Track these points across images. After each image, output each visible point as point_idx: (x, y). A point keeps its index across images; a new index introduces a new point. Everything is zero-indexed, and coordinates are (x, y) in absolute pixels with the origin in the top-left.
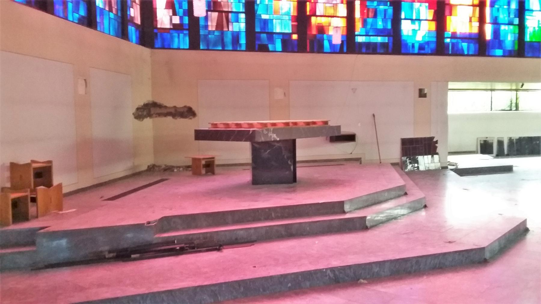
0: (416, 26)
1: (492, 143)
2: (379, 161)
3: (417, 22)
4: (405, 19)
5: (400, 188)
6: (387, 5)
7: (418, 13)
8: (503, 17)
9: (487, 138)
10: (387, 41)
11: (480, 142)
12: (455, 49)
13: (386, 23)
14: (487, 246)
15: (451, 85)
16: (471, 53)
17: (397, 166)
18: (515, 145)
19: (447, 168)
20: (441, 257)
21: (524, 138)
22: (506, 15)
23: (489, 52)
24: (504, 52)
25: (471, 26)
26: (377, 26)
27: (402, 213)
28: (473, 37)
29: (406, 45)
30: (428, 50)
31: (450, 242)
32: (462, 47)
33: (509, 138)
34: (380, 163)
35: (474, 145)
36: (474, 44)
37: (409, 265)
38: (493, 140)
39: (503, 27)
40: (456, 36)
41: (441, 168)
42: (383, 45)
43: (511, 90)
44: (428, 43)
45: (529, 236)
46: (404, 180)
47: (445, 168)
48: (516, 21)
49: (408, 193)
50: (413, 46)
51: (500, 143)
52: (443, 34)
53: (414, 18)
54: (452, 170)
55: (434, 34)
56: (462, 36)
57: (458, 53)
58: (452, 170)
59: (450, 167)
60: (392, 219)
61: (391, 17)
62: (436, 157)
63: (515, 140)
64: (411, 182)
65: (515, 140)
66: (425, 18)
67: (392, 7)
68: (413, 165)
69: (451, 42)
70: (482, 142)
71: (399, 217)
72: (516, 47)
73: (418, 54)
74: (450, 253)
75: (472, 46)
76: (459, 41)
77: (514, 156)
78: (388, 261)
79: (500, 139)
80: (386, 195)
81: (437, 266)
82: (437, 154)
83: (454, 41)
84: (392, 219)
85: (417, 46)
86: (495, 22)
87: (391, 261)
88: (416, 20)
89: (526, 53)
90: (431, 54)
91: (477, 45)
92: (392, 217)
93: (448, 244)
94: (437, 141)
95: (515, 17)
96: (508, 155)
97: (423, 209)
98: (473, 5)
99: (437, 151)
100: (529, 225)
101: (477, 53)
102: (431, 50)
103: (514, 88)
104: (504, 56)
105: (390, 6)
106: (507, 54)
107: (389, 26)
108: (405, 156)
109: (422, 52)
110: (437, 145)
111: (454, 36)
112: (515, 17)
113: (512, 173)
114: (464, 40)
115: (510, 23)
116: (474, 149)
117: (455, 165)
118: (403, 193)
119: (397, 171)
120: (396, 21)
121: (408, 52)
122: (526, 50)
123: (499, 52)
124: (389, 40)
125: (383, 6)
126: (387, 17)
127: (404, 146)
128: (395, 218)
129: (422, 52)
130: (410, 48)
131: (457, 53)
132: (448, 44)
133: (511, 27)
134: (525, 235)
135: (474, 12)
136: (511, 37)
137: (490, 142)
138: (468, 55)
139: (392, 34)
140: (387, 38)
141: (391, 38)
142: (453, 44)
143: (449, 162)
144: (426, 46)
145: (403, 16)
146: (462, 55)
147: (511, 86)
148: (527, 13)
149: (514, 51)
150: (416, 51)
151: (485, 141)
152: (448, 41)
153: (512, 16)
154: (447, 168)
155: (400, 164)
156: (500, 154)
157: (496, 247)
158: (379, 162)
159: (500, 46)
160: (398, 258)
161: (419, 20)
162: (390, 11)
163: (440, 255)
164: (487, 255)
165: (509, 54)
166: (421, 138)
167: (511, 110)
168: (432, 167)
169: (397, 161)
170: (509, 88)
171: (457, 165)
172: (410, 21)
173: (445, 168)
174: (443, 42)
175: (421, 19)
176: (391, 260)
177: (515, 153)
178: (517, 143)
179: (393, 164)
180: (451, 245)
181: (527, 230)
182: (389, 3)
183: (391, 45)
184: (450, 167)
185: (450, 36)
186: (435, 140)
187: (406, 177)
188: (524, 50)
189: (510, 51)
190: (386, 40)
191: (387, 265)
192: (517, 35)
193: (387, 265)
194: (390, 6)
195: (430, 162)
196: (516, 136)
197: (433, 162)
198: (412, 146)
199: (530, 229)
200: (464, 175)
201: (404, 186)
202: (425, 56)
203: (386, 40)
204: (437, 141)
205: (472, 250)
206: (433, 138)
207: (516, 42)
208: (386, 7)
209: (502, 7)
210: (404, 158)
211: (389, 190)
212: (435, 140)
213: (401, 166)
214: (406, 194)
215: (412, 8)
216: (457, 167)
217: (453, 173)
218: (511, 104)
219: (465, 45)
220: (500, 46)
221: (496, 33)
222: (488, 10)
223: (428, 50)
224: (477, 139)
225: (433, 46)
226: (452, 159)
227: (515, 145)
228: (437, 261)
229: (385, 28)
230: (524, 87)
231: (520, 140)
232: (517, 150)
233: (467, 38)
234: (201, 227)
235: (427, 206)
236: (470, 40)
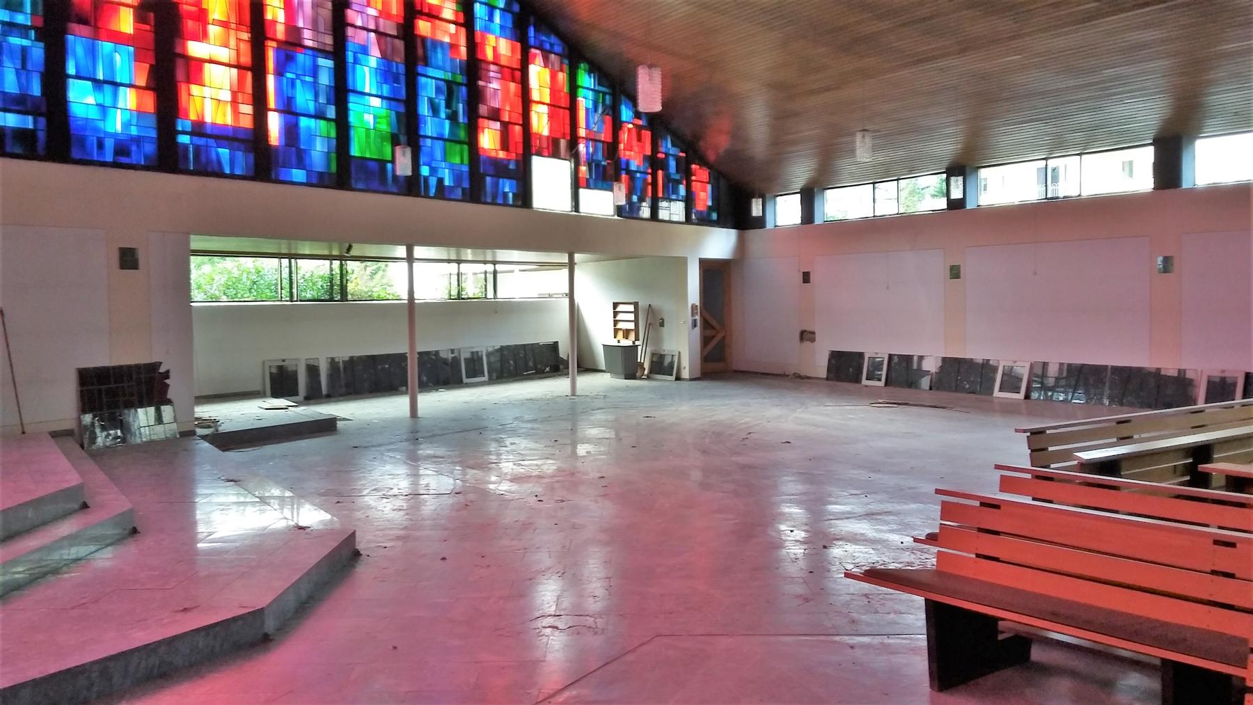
0: (106, 97)
1: (296, 372)
2: (20, 428)
3: (108, 88)
4: (78, 77)
5: (67, 494)
6: (27, 37)
7: (111, 65)
8: (304, 99)
9: (284, 361)
10: (31, 126)
11: (270, 369)
12: (203, 159)
13: (29, 81)
14: (270, 605)
15: (196, 242)
16: (238, 172)
17: (70, 438)
18: (342, 375)
19: (192, 433)
20: (163, 649)
21: (359, 358)
22: (310, 96)
23: (277, 175)
24: (310, 173)
25: (236, 112)
26: (3, 87)
27: (74, 557)
28: (242, 136)
29: (82, 141)
30: (136, 157)
31: (185, 610)
32: (218, 155)
33: (329, 360)
34: (24, 433)
35: (257, 376)
36: (246, 151)
37: (82, 681)
38: (297, 365)
39: (304, 122)
40: (204, 131)
41: (178, 436)
42: (21, 135)
43: (449, 261)
44: (138, 140)
45: (363, 571)
46: (82, 474)
47: (188, 434)
48: (331, 112)
49: (89, 505)
50: (101, 145)
51: (313, 370)
52: (174, 125)
53: (100, 76)
54: (204, 437)
55: (152, 121)
56: (215, 132)
57: (209, 170)
58: (204, 437)
59: (200, 431)
60: (45, 575)
61: (42, 69)
62: (167, 411)
63: (341, 365)
64: (100, 477)
65: (341, 365)
66: (127, 82)
67: (42, 45)
68: (111, 432)
69: (191, 143)
70: (274, 371)
71: (65, 569)
72: (334, 168)
73: (115, 165)
74: (185, 635)
75: (240, 155)
76: (211, 142)
77: (341, 398)
78: (23, 685)
79: (311, 363)
80: (30, 515)
81: (155, 672)
82: (169, 402)
83: (201, 141)
84: (45, 575)
85: (109, 144)
86: (289, 110)
87: (35, 683)
88: (105, 82)
89: (353, 182)
90: (146, 168)
91: (252, 156)
92: (45, 570)
93: (179, 616)
94: (168, 372)
95: (329, 102)
96: (331, 397)
97: (130, 540)
98: (238, 66)
99: (169, 396)
100: (361, 545)
101: (252, 173)
102: (146, 157)
103: (453, 257)
104: (308, 184)
105: (38, 39)
106: (315, 181)
107: (36, 89)
108: (90, 411)
109: (124, 160)
110: (167, 381)
111: (199, 129)
112: (329, 102)
113: (336, 434)
114: (221, 142)
115: (319, 115)
116: (258, 387)
117: (212, 425)
118: (76, 506)
119: (67, 455)
120: (55, 79)
121: (89, 158)
122: (353, 175)
123: (298, 175)
124: (35, 122)
125: (19, 39)
126: (29, 67)
127: (85, 388)
128: (55, 571)
129: (124, 160)
130: (93, 145)
131: (210, 170)
132: (186, 147)
133: (323, 123)
134: (353, 566)
135: (241, 80)
136: (323, 145)
137: (290, 369)
138: (232, 176)
139: (44, 109)
140: (30, 118)
141: (42, 121)
142: (197, 149)
143: (197, 419)
144: (134, 148)
145: (71, 70)
146: (220, 175)
147: (330, 249)
148: (352, 98)
149: (330, 174)
150: (109, 157)
151: (280, 368)
152: (184, 139)
153: (322, 100)
154: (192, 433)
155: (76, 431)
156: (314, 396)
157: (291, 602)
158: (21, 431)
159: (301, 159)
160: (53, 670)
161: (116, 85)
162: (38, 52)
163: (159, 643)
164: (270, 625)
165: (320, 181)
166: (129, 367)
167: (331, 300)
168: (160, 432)
169: (70, 424)
170: (326, 252)
171: (216, 426)
172: (89, 83)
173: (188, 434)
174: (175, 144)
175: (118, 80)
176: (34, 680)
177: (343, 390)
178: (345, 368)
179: (55, 435)
180: (189, 615)
181: (357, 554)
182: (32, 33)
183: (42, 135)
184: (200, 431)
185: (189, 129)
186: (162, 370)
187: (90, 465)
188: (348, 172)
189: (321, 175)
190: (29, 122)
191: (26, 693)
192: (334, 142)
193: (26, 693)
194: (38, 39)
195: (152, 422)
196: (343, 353)
197: (159, 419)
198: (111, 386)
199: (362, 552)
200: (232, 447)
201: (80, 488)
202: (132, 171)
203: (29, 122)
204: (168, 372)
205: (235, 619)
206: (157, 365)
207: (334, 156)
208: (25, 42)
209: (302, 77)
210: (87, 418)
211: (37, 503)
212: (162, 370)
213: (79, 438)
214: (85, 506)
215: (92, 53)
216: (217, 431)
217: (206, 445)
218: (332, 286)
219: (224, 152)
220: (301, 164)
221: (291, 131)
222: (271, 81)
223: (136, 157)
224: (264, 362)
225: (150, 148)
226: (205, 411)
227: (342, 375)
228: (154, 661)
229: (22, 93)
230: (354, 252)
231: (352, 362)
232: (347, 385)
233: (223, 136)
234: (1236, 449)
235: (138, 529)
236: (236, 144)
